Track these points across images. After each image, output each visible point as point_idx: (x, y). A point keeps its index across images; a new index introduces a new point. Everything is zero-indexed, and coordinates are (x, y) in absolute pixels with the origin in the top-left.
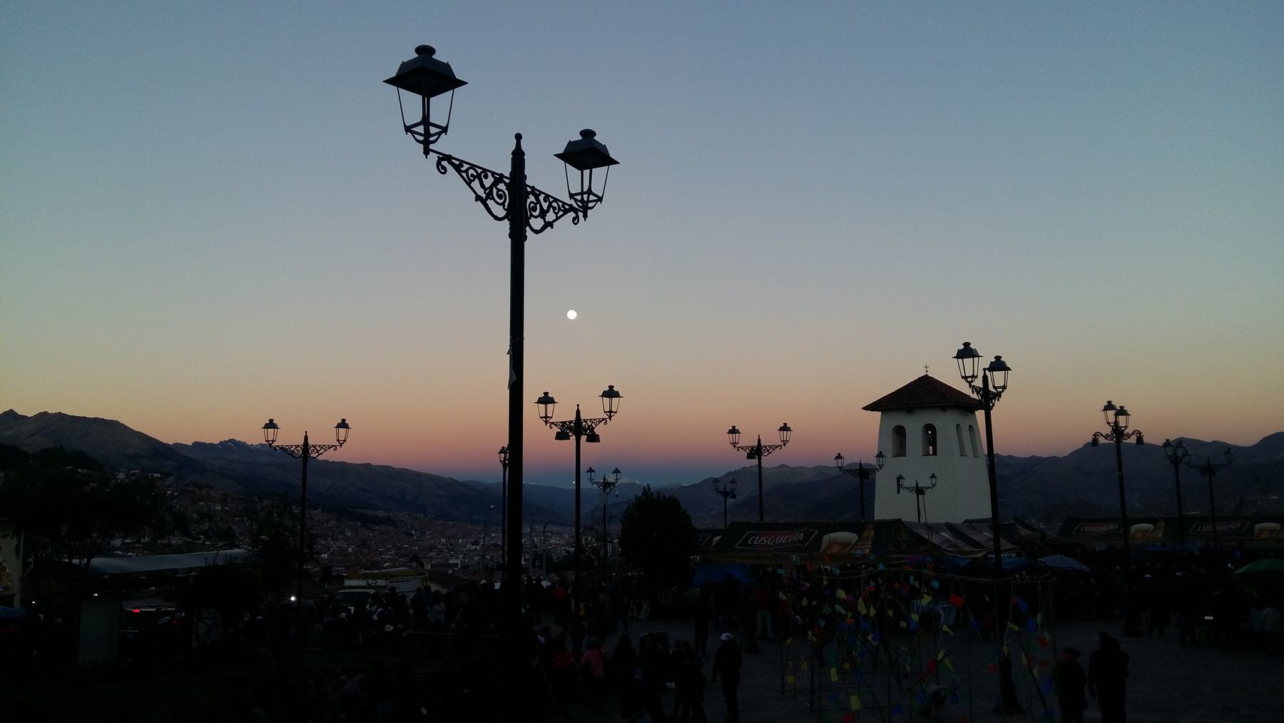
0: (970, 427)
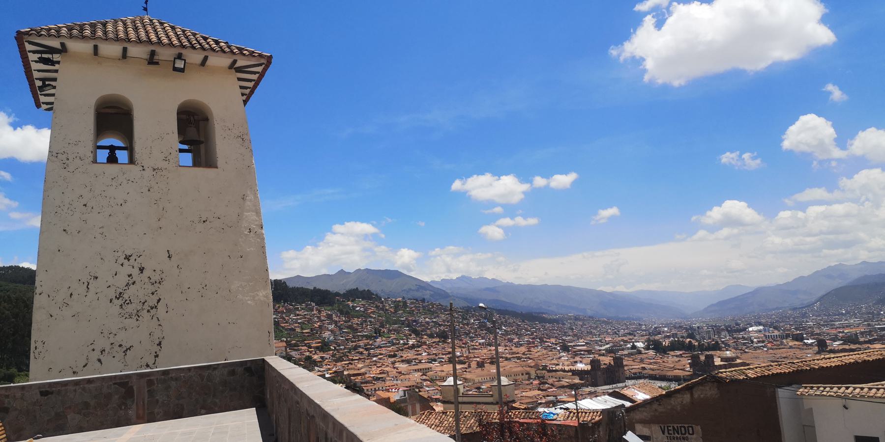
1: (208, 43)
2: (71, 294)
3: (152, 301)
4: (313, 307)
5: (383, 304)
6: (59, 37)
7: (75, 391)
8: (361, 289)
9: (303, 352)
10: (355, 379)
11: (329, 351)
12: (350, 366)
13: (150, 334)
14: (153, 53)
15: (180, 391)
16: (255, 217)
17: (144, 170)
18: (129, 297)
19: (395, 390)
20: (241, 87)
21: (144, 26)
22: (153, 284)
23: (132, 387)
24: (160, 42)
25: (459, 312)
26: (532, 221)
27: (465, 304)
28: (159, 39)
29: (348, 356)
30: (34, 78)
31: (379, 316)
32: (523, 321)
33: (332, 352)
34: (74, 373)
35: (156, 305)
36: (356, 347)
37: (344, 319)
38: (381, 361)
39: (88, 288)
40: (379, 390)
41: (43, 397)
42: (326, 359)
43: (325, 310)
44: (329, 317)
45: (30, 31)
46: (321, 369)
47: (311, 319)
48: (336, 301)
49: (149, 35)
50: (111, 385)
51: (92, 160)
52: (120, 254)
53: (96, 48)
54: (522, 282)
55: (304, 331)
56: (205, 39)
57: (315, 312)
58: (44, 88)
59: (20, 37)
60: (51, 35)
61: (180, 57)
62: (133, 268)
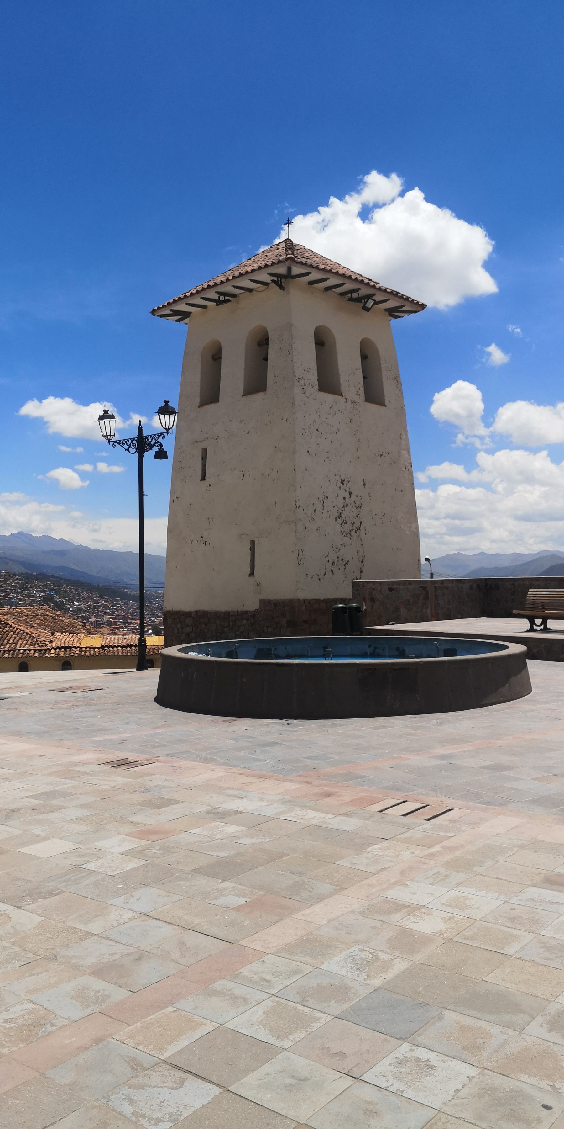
0: (37, 837)
25: (17, 579)
26: (116, 469)
27: (22, 570)
32: (101, 596)
39: (323, 506)
54: (100, 547)
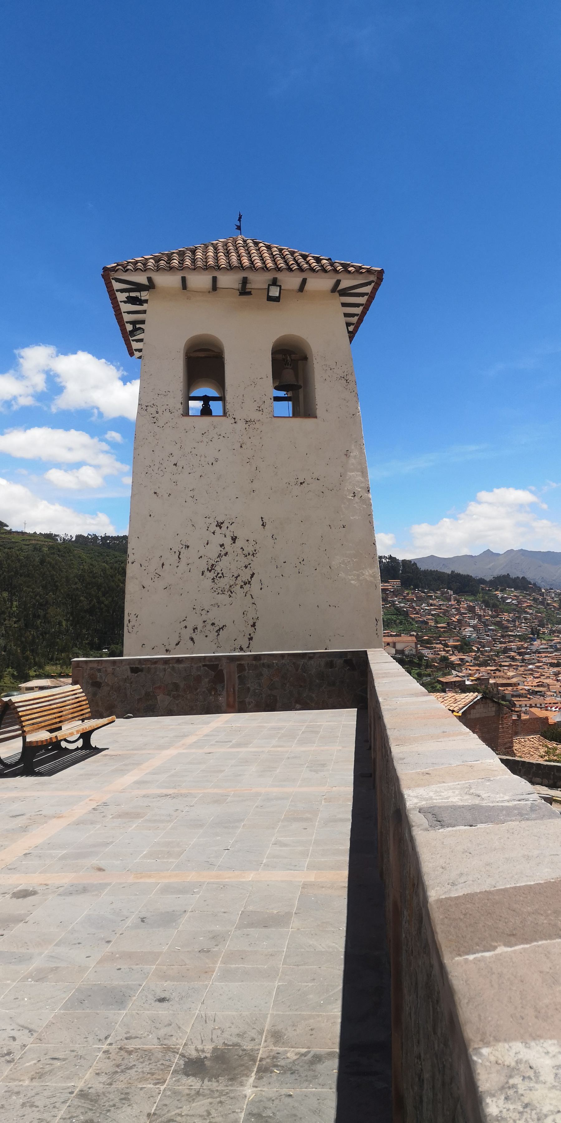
1: (307, 263)
2: (163, 565)
3: (245, 576)
4: (451, 595)
5: (543, 596)
6: (145, 271)
7: (165, 670)
8: (513, 576)
9: (438, 651)
10: (504, 690)
11: (471, 652)
12: (498, 673)
13: (244, 614)
14: (245, 281)
15: (272, 680)
16: (360, 478)
17: (235, 423)
18: (221, 570)
19: (555, 708)
20: (346, 315)
21: (237, 249)
22: (246, 556)
23: (222, 671)
24: (252, 266)
28: (252, 262)
29: (494, 660)
30: (125, 321)
31: (536, 612)
33: (474, 654)
34: (167, 651)
35: (250, 580)
36: (506, 650)
37: (490, 613)
38: (539, 670)
39: (180, 558)
40: (536, 706)
41: (133, 674)
42: (467, 662)
43: (466, 600)
44: (471, 609)
45: (116, 266)
46: (460, 674)
47: (448, 611)
48: (480, 590)
49: (241, 259)
50: (200, 667)
51: (182, 413)
52: (211, 520)
53: (184, 279)
55: (439, 625)
56: (305, 257)
57: (453, 602)
58: (135, 333)
59: (107, 274)
60: (138, 269)
61: (274, 282)
62: (225, 536)
